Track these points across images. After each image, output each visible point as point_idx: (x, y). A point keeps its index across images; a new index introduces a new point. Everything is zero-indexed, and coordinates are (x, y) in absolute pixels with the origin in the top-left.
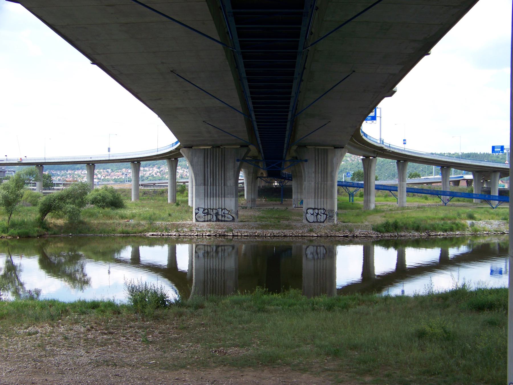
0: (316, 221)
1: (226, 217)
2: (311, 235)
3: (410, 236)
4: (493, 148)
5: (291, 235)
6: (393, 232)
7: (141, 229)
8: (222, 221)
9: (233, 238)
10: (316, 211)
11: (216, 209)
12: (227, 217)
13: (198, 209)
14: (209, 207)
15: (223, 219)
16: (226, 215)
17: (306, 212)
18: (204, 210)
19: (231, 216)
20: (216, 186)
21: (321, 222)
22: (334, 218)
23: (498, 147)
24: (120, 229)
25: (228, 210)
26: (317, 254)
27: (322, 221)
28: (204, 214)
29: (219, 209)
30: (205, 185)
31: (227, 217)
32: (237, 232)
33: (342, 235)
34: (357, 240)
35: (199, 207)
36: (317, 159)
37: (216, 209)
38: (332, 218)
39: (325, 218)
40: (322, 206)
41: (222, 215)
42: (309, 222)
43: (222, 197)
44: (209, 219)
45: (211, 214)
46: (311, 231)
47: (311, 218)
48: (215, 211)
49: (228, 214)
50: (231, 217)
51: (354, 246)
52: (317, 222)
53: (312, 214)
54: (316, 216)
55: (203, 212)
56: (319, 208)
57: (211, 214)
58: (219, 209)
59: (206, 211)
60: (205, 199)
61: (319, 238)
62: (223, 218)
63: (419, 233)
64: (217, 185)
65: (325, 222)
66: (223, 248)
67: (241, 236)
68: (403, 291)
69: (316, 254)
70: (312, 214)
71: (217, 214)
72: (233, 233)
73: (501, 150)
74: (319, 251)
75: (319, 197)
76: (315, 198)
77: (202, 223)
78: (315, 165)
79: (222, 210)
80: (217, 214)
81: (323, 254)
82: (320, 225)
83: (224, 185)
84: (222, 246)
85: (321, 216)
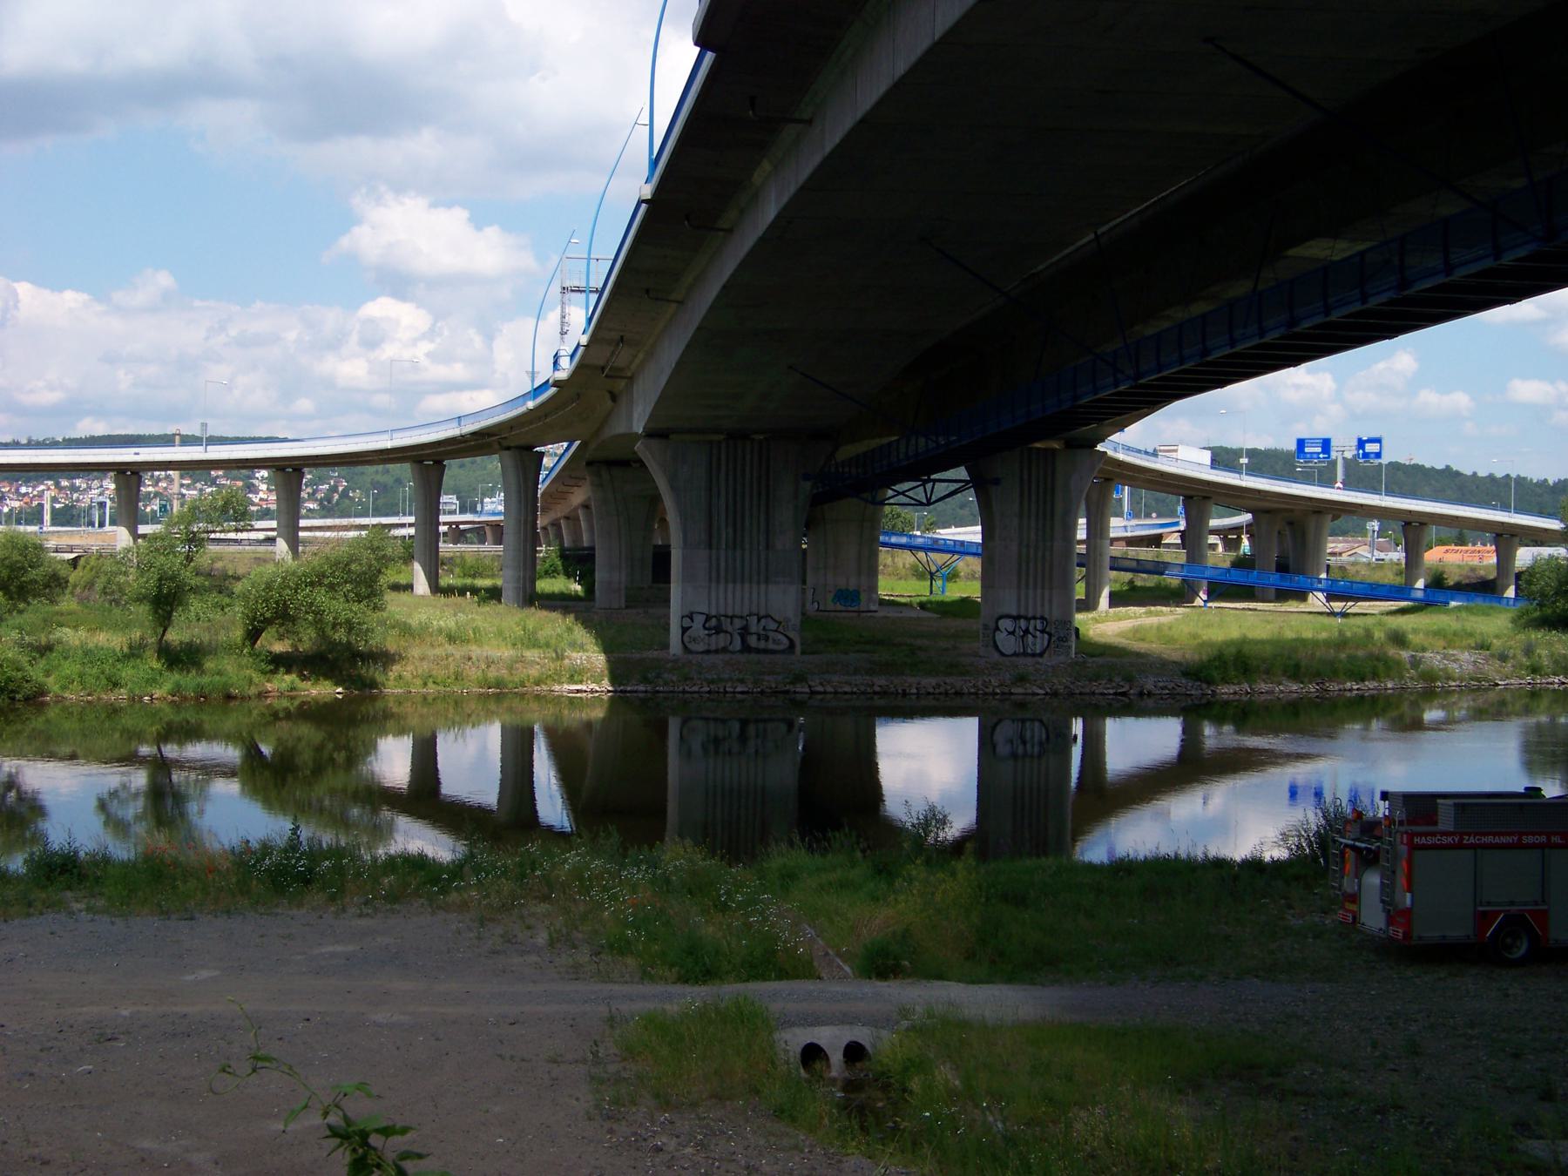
0: (1022, 650)
1: (771, 641)
2: (1030, 691)
3: (1282, 692)
4: (1301, 443)
5: (972, 690)
6: (1239, 684)
7: (534, 672)
8: (758, 651)
9: (809, 698)
10: (1023, 623)
11: (742, 617)
12: (774, 640)
13: (691, 617)
14: (723, 612)
15: (762, 645)
16: (771, 634)
17: (992, 625)
18: (708, 618)
19: (786, 636)
20: (743, 549)
21: (1034, 655)
22: (1070, 643)
23: (1313, 441)
24: (473, 673)
25: (777, 618)
26: (1024, 743)
27: (1038, 651)
28: (706, 632)
29: (749, 615)
30: (710, 547)
31: (774, 640)
32: (821, 684)
33: (1111, 691)
34: (1150, 702)
35: (692, 610)
36: (1026, 477)
37: (742, 617)
38: (1066, 644)
39: (1046, 643)
40: (1039, 609)
41: (759, 635)
42: (1002, 654)
43: (1035, 588)
44: (722, 644)
45: (726, 632)
46: (1021, 679)
47: (1007, 643)
48: (738, 623)
49: (776, 631)
50: (785, 641)
51: (951, 719)
52: (1025, 654)
53: (1010, 633)
54: (1022, 637)
55: (704, 626)
56: (1030, 615)
57: (726, 632)
58: (749, 615)
59: (713, 622)
60: (710, 588)
61: (1048, 697)
62: (763, 642)
63: (1302, 686)
64: (747, 546)
65: (1046, 655)
66: (761, 726)
67: (836, 693)
68: (1111, 851)
69: (1019, 741)
70: (1010, 633)
71: (745, 632)
72: (810, 687)
73: (1323, 452)
74: (1028, 734)
75: (722, 581)
76: (1019, 587)
77: (700, 657)
78: (1022, 495)
79: (759, 620)
80: (745, 632)
81: (1041, 744)
82: (1038, 663)
83: (767, 547)
84: (757, 721)
85: (1034, 637)
